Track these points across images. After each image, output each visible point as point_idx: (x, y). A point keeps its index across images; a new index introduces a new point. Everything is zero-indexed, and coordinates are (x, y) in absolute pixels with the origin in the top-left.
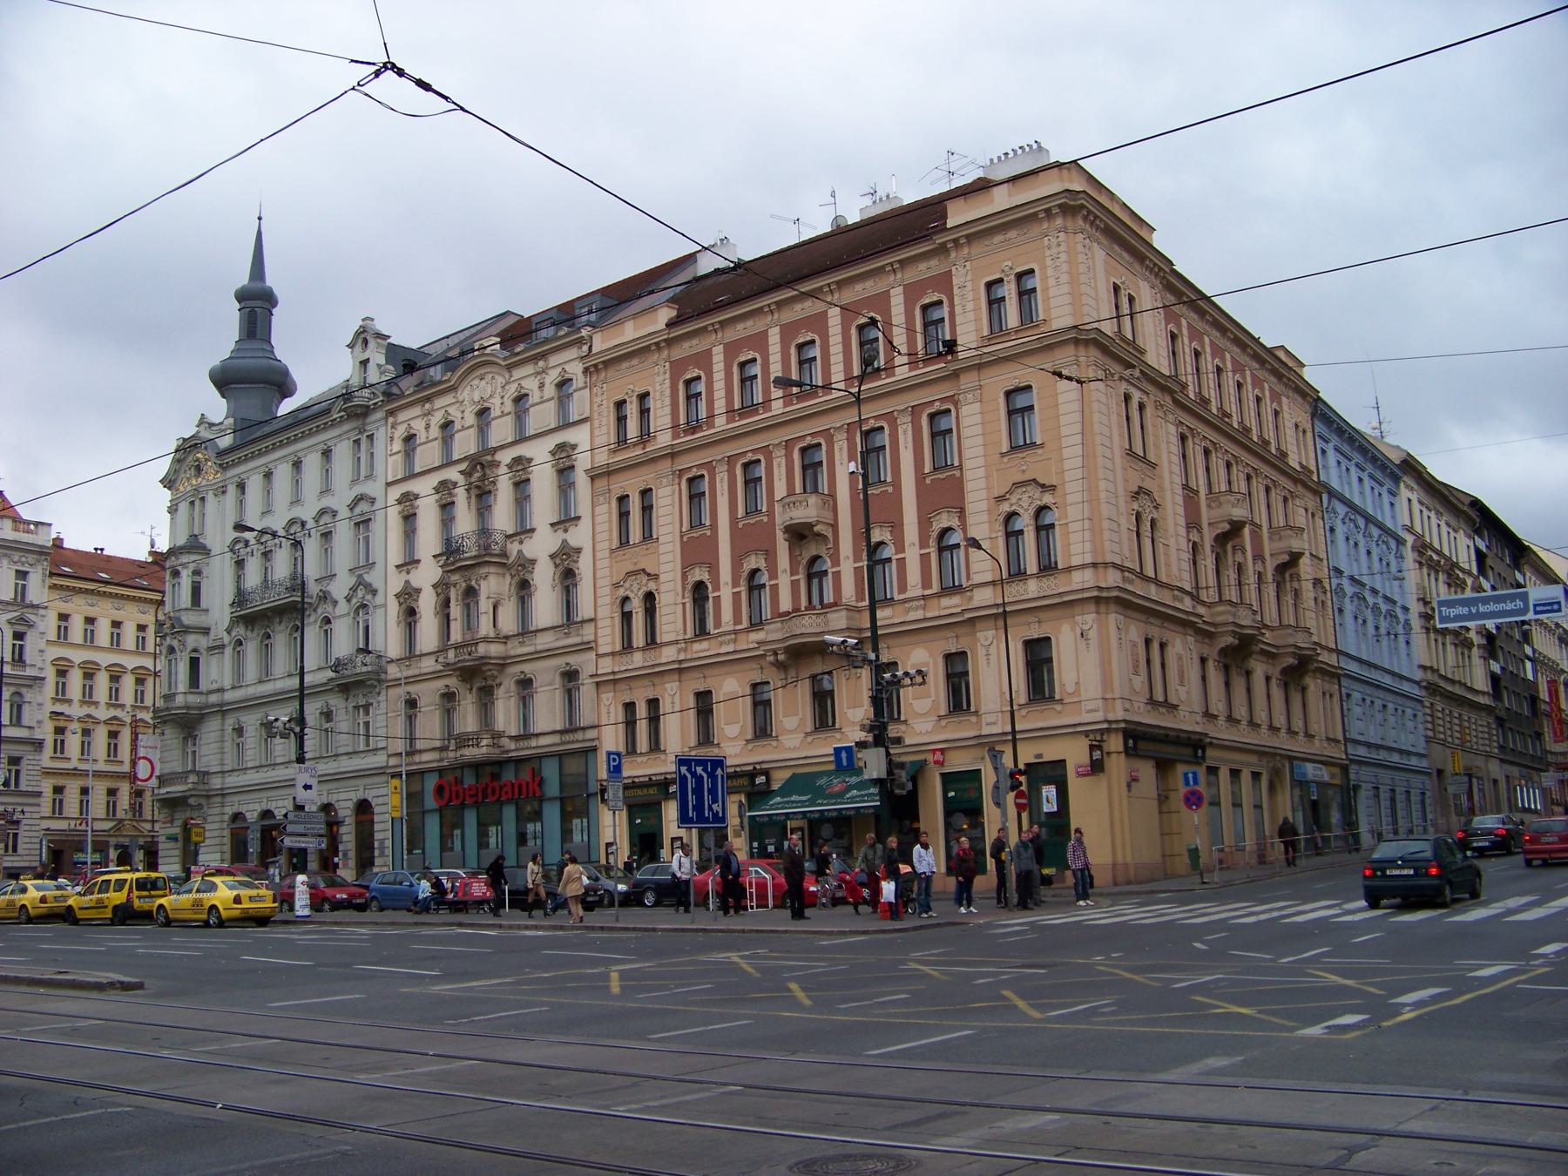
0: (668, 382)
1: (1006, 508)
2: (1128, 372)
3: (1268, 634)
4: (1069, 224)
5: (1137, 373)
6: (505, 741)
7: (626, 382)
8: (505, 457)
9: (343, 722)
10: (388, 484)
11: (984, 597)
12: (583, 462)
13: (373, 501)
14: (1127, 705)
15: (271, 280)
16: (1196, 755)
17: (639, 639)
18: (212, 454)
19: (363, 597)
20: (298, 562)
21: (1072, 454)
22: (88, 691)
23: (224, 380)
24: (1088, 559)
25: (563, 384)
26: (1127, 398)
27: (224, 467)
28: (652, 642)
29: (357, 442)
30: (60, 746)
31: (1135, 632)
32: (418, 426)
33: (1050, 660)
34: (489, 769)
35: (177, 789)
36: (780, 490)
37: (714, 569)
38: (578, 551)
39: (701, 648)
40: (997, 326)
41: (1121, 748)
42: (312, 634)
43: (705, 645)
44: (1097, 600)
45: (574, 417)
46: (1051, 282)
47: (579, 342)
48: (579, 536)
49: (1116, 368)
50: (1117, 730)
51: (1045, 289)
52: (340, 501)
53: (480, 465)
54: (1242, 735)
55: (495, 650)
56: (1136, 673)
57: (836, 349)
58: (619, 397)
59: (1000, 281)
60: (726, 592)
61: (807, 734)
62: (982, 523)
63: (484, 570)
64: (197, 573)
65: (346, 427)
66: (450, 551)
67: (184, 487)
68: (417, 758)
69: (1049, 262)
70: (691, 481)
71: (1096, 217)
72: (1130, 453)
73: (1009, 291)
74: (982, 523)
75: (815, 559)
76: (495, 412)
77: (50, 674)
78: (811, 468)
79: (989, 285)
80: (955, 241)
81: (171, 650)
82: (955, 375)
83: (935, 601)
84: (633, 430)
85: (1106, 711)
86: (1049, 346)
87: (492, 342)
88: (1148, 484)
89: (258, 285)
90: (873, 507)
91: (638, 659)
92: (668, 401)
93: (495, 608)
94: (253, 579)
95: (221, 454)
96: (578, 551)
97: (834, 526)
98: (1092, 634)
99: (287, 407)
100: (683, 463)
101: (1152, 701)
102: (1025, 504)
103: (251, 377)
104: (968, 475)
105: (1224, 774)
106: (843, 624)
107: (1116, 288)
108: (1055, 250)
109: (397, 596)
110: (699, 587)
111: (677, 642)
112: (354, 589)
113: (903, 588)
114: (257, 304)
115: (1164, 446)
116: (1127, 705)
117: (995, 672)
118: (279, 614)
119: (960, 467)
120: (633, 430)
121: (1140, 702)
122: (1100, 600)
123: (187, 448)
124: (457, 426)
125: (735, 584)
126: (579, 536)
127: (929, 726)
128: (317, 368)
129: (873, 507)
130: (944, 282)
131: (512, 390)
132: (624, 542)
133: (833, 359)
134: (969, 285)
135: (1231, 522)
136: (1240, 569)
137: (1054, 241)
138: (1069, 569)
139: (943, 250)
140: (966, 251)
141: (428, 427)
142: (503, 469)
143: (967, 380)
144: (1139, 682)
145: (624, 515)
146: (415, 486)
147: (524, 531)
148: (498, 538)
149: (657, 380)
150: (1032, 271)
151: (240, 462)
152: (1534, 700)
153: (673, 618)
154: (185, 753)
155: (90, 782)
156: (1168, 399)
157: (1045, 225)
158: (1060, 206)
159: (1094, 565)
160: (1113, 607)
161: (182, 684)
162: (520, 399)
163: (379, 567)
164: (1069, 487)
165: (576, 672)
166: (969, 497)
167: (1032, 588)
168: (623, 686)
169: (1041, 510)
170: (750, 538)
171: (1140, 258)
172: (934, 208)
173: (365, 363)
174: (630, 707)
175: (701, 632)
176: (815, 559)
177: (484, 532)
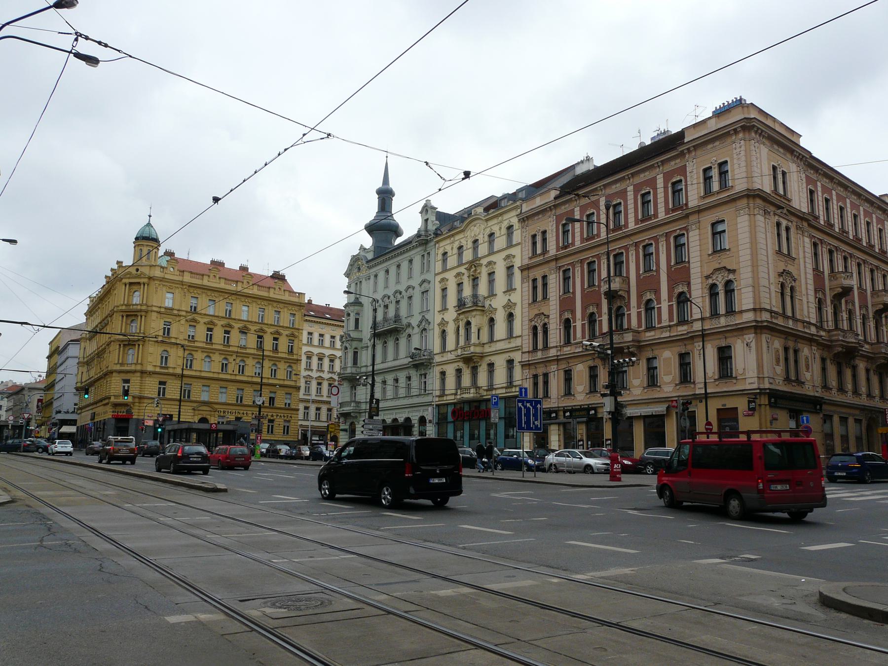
0: (555, 226)
1: (710, 281)
2: (779, 211)
3: (867, 346)
4: (747, 136)
5: (785, 211)
6: (481, 391)
7: (536, 226)
8: (484, 262)
9: (415, 382)
10: (436, 275)
11: (697, 326)
12: (517, 263)
13: (429, 282)
14: (771, 381)
15: (392, 185)
17: (540, 345)
18: (364, 262)
19: (424, 327)
20: (397, 310)
21: (745, 254)
22: (320, 365)
23: (371, 229)
24: (751, 306)
25: (510, 228)
26: (778, 225)
27: (369, 268)
28: (546, 347)
29: (423, 256)
30: (307, 389)
31: (777, 344)
32: (448, 249)
33: (731, 357)
34: (475, 404)
35: (346, 409)
36: (604, 274)
37: (573, 312)
38: (515, 304)
39: (567, 350)
40: (708, 192)
41: (767, 403)
42: (403, 341)
43: (569, 348)
44: (755, 327)
45: (514, 243)
46: (736, 166)
47: (515, 208)
48: (516, 297)
49: (771, 209)
50: (765, 394)
51: (733, 171)
52: (415, 282)
53: (474, 264)
54: (849, 398)
55: (478, 350)
57: (631, 206)
58: (533, 233)
59: (710, 168)
60: (578, 324)
61: (676, 385)
62: (698, 292)
63: (474, 313)
64: (358, 314)
65: (419, 249)
66: (461, 304)
67: (354, 277)
68: (445, 398)
69: (735, 156)
70: (564, 271)
71: (762, 131)
72: (779, 252)
73: (715, 173)
74: (698, 292)
75: (619, 308)
76: (480, 241)
77: (304, 358)
78: (618, 264)
79: (705, 170)
80: (688, 149)
81: (346, 348)
82: (687, 216)
83: (675, 328)
85: (759, 384)
86: (733, 200)
87: (480, 210)
88: (790, 268)
89: (385, 187)
90: (649, 282)
91: (539, 355)
92: (554, 234)
93: (479, 330)
94: (380, 317)
95: (368, 262)
96: (515, 304)
97: (628, 292)
98: (753, 345)
99: (398, 241)
100: (561, 263)
101: (787, 379)
103: (382, 228)
104: (692, 266)
105: (836, 419)
106: (630, 339)
107: (774, 168)
108: (738, 150)
109: (439, 325)
110: (567, 321)
111: (556, 347)
112: (421, 322)
113: (660, 322)
114: (385, 196)
115: (801, 249)
116: (771, 381)
117: (705, 364)
118: (388, 333)
119: (689, 262)
121: (780, 379)
122: (758, 328)
123: (355, 260)
124: (464, 248)
125: (639, 307)
126: (516, 297)
127: (671, 389)
128: (409, 224)
129: (649, 282)
130: (683, 170)
131: (488, 232)
132: (535, 300)
133: (629, 211)
134: (695, 171)
135: (843, 288)
136: (851, 313)
137: (738, 145)
138: (741, 312)
139: (682, 155)
140: (693, 154)
141: (452, 249)
142: (484, 267)
143: (693, 218)
144: (780, 369)
145: (535, 288)
146: (512, 251)
147: (492, 294)
148: (481, 298)
149: (549, 224)
150: (726, 162)
151: (376, 265)
153: (555, 336)
154: (351, 394)
155: (320, 406)
156: (805, 224)
157: (734, 137)
158: (741, 127)
159: (754, 310)
161: (350, 363)
162: (491, 235)
163: (432, 311)
165: (513, 360)
166: (692, 277)
167: (723, 321)
168: (532, 367)
170: (590, 298)
171: (792, 152)
172: (681, 135)
173: (426, 220)
174: (535, 377)
175: (568, 342)
176: (619, 308)
177: (475, 296)
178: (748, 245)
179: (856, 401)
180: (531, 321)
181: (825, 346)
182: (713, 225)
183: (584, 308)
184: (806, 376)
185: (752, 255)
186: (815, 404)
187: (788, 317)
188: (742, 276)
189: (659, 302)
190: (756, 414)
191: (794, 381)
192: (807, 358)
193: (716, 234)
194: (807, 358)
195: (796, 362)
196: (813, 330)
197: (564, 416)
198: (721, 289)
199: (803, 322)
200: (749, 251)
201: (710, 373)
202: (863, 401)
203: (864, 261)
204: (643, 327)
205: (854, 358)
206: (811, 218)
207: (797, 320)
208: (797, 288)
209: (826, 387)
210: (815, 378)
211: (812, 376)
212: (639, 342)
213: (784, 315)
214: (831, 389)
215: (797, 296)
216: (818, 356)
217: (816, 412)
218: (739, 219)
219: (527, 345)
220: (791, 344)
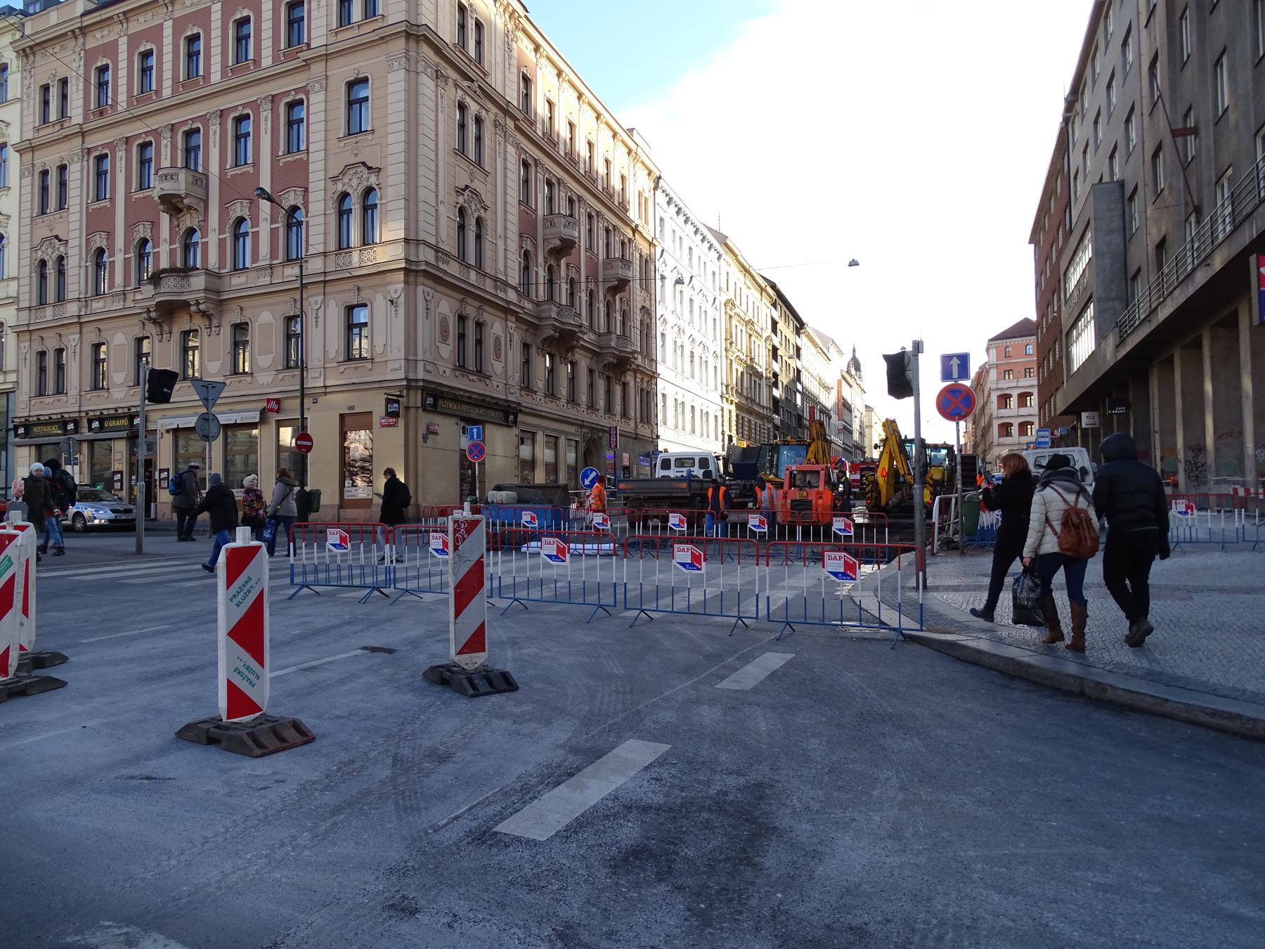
1: (340, 187)
7: (49, 67)
16: (507, 419)
17: (51, 295)
37: (110, 235)
39: (97, 305)
50: (417, 388)
54: (560, 408)
56: (444, 339)
72: (461, 151)
82: (307, 64)
84: (53, 115)
85: (407, 371)
91: (49, 312)
97: (206, 202)
100: (91, 142)
101: (461, 367)
102: (354, 187)
113: (255, 258)
116: (429, 368)
120: (53, 115)
125: (221, 231)
135: (562, 240)
143: (317, 69)
144: (447, 350)
145: (44, 189)
152: (800, 418)
160: (421, 279)
164: (391, 170)
166: (312, 177)
169: (369, 191)
178: (402, 126)
179: (571, 413)
180: (33, 249)
181: (531, 326)
182: (351, 85)
183: (130, 227)
184: (495, 367)
185: (407, 143)
186: (507, 413)
187: (469, 267)
188: (391, 181)
189: (256, 224)
190: (401, 422)
191: (472, 373)
192: (497, 340)
193: (354, 103)
194: (497, 340)
195: (479, 342)
196: (512, 296)
197: (90, 429)
198: (355, 204)
199: (496, 280)
200: (402, 136)
201: (332, 355)
202: (582, 414)
203: (598, 213)
204: (228, 269)
205: (571, 349)
206: (520, 116)
207: (485, 275)
208: (489, 222)
209: (527, 387)
210: (510, 373)
211: (506, 367)
212: (219, 293)
213: (461, 258)
214: (535, 392)
215: (488, 237)
216: (516, 338)
217: (506, 424)
218: (392, 77)
219: (28, 296)
220: (470, 311)
